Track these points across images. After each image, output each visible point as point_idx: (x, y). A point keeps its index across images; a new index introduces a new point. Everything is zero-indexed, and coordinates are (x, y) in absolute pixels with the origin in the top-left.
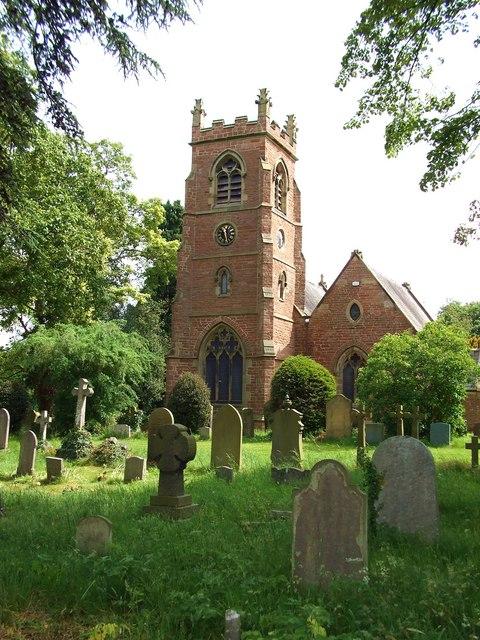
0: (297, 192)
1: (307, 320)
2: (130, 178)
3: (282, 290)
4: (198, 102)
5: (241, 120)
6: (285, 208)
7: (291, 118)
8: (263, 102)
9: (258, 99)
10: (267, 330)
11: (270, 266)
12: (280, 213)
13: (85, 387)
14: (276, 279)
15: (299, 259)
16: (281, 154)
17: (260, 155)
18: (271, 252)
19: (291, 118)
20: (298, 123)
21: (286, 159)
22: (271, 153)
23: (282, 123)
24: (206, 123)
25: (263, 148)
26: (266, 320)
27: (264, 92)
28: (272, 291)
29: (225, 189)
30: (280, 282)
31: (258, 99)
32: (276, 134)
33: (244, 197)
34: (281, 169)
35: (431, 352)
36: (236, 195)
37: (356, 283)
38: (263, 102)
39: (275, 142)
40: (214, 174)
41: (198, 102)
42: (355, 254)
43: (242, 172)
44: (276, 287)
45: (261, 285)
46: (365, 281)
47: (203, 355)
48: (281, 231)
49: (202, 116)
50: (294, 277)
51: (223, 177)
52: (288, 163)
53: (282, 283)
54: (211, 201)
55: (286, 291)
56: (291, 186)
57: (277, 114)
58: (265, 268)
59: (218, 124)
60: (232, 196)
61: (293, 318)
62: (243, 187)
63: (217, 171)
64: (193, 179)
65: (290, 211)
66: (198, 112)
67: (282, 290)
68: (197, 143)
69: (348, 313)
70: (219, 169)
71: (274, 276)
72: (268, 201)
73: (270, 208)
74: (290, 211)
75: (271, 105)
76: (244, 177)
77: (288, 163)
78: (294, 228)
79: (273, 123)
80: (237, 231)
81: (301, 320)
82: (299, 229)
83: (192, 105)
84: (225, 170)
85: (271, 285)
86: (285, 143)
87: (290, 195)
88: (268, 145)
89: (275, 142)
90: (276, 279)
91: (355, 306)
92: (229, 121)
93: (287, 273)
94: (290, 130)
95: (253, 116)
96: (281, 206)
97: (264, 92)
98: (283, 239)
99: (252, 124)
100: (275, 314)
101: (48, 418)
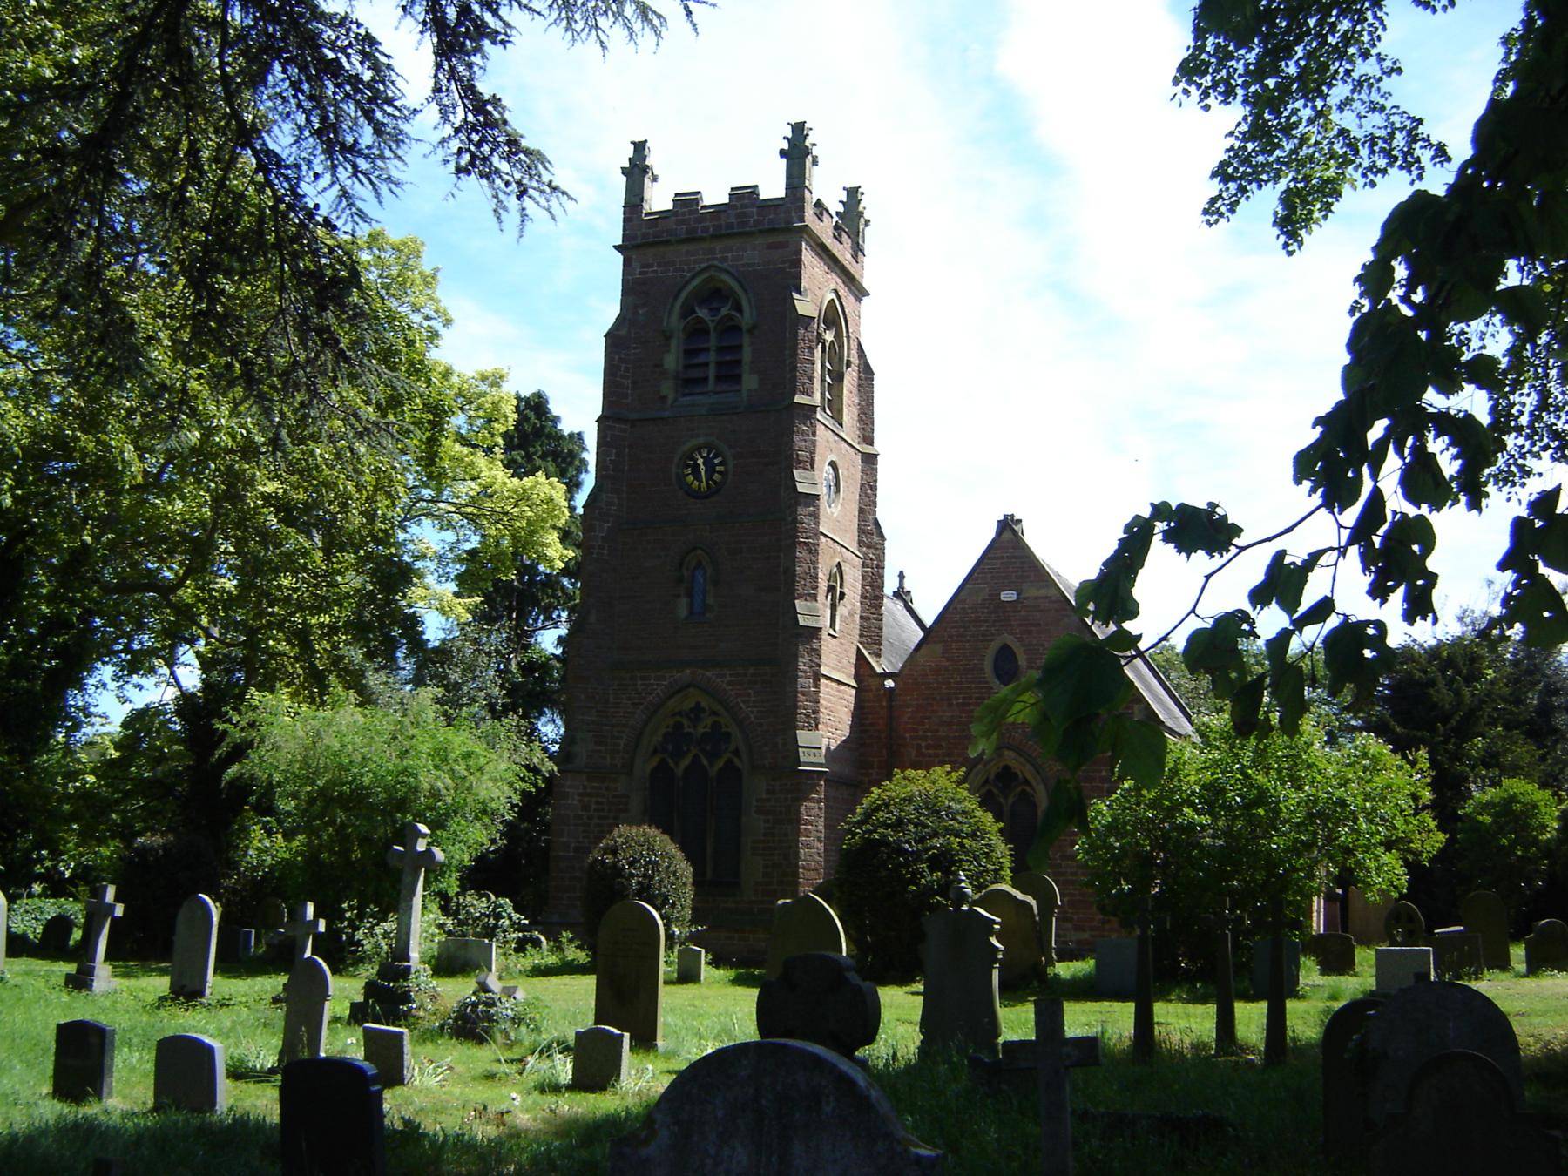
0: (867, 372)
1: (889, 683)
2: (437, 325)
3: (834, 608)
4: (640, 147)
5: (744, 197)
6: (840, 411)
7: (853, 194)
8: (797, 152)
9: (785, 145)
10: (804, 703)
11: (813, 550)
12: (830, 423)
13: (421, 846)
14: (823, 585)
15: (871, 536)
16: (835, 281)
17: (792, 280)
18: (815, 516)
19: (853, 194)
20: (868, 205)
21: (843, 292)
22: (813, 270)
23: (835, 206)
24: (659, 199)
25: (798, 263)
26: (804, 682)
27: (799, 130)
28: (813, 612)
29: (701, 359)
30: (831, 589)
31: (785, 145)
32: (824, 230)
33: (750, 382)
34: (833, 317)
35: (73, 603)
36: (729, 374)
37: (1008, 596)
38: (797, 152)
39: (823, 251)
40: (674, 321)
41: (640, 147)
42: (1008, 527)
43: (747, 318)
44: (823, 602)
45: (791, 596)
46: (1031, 592)
47: (645, 766)
48: (833, 465)
49: (647, 181)
50: (858, 575)
51: (697, 331)
52: (848, 300)
53: (833, 591)
54: (667, 388)
55: (842, 610)
56: (855, 359)
57: (825, 187)
58: (801, 553)
59: (687, 202)
60: (719, 379)
61: (857, 677)
62: (747, 355)
63: (684, 316)
64: (623, 332)
65: (850, 414)
66: (637, 171)
67: (834, 608)
68: (637, 247)
69: (988, 665)
70: (688, 311)
71: (820, 575)
72: (809, 393)
73: (813, 408)
74: (850, 414)
75: (815, 162)
76: (751, 330)
77: (848, 300)
78: (859, 458)
79: (819, 204)
80: (731, 463)
81: (874, 682)
82: (870, 460)
83: (626, 153)
84: (702, 313)
85: (814, 597)
86: (843, 252)
87: (851, 378)
88: (808, 256)
89: (823, 251)
90: (823, 585)
91: (1005, 654)
92: (715, 195)
93: (845, 567)
94: (851, 218)
95: (773, 186)
96: (834, 406)
97: (799, 130)
98: (837, 485)
99: (773, 204)
100: (824, 670)
101: (315, 923)
